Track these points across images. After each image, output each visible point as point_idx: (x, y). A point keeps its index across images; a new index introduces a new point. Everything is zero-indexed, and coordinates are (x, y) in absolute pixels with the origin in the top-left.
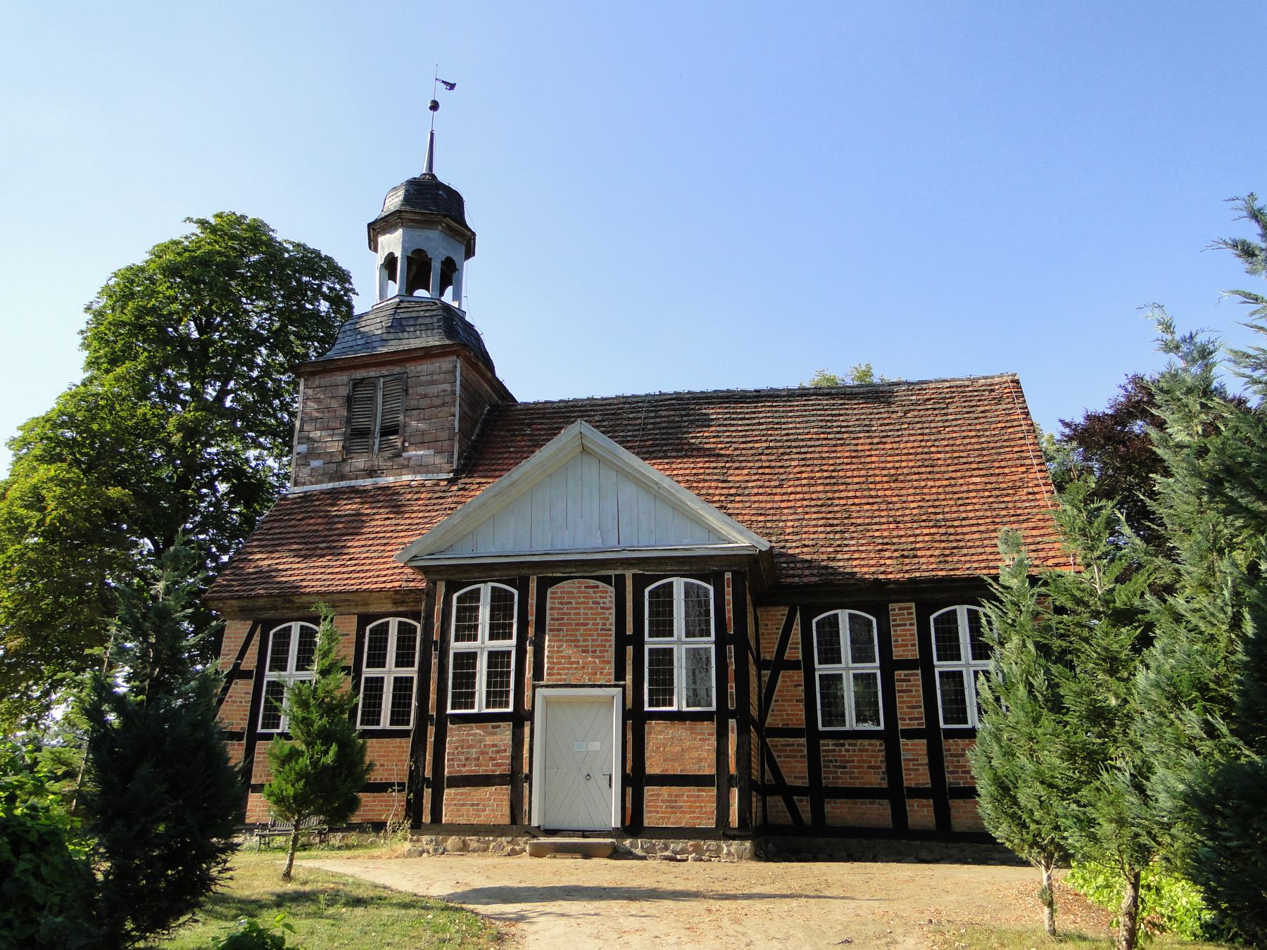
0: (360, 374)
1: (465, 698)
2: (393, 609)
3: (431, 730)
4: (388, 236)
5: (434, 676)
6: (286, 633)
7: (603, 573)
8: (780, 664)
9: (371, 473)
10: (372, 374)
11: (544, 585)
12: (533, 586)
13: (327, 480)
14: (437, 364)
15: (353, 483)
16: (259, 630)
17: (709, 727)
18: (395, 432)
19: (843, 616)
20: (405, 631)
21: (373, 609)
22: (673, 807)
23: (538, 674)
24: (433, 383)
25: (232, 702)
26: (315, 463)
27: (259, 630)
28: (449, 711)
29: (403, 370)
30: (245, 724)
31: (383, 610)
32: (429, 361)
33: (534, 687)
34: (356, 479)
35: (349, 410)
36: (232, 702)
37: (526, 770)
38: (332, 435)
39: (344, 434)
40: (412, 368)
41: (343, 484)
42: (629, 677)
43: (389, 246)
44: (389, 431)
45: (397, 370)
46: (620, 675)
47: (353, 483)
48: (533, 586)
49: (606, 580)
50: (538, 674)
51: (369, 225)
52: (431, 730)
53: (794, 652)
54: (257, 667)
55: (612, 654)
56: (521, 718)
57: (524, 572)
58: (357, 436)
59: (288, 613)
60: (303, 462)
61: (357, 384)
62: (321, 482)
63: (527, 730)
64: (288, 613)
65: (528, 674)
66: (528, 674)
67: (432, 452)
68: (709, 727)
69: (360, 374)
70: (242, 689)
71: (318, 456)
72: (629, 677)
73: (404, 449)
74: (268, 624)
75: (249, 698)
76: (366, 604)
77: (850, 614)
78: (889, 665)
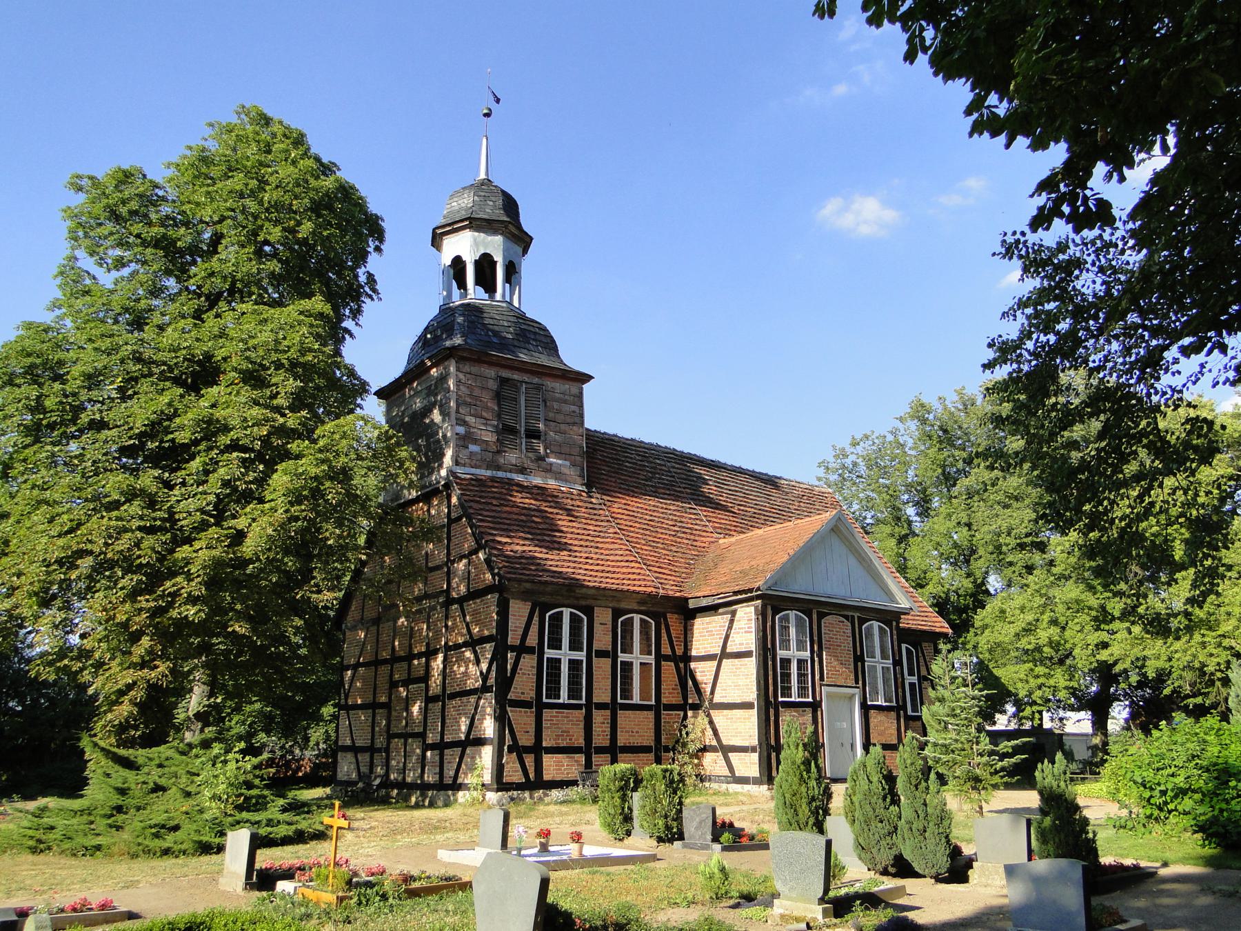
0: (506, 374)
1: (787, 691)
2: (636, 607)
3: (772, 711)
4: (482, 235)
5: (770, 673)
6: (557, 618)
7: (846, 613)
8: (522, 649)
9: (522, 470)
10: (516, 377)
11: (821, 616)
12: (815, 616)
13: (485, 466)
14: (567, 386)
15: (509, 475)
16: (537, 613)
17: (893, 714)
18: (538, 438)
19: (566, 612)
20: (574, 620)
21: (624, 605)
22: (559, 764)
23: (822, 678)
24: (565, 402)
25: (524, 674)
26: (474, 448)
27: (537, 613)
28: (780, 699)
29: (540, 382)
30: (533, 694)
31: (630, 607)
32: (561, 381)
33: (821, 685)
34: (510, 472)
35: (499, 405)
36: (524, 674)
37: (821, 741)
38: (486, 424)
39: (496, 427)
40: (550, 383)
41: (500, 474)
42: (860, 682)
43: (486, 247)
44: (533, 434)
45: (536, 380)
46: (857, 682)
47: (509, 475)
48: (815, 616)
49: (846, 617)
50: (822, 678)
51: (531, 239)
52: (772, 711)
53: (532, 640)
54: (538, 644)
55: (852, 666)
56: (815, 706)
57: (811, 606)
58: (507, 431)
59: (560, 599)
60: (462, 443)
61: (504, 381)
62: (476, 467)
63: (819, 713)
64: (560, 599)
65: (817, 677)
66: (817, 677)
67: (568, 463)
68: (893, 714)
69: (506, 374)
70: (528, 662)
71: (475, 441)
72: (860, 682)
73: (547, 455)
74: (545, 608)
75: (534, 670)
76: (619, 601)
77: (641, 619)
78: (659, 657)
